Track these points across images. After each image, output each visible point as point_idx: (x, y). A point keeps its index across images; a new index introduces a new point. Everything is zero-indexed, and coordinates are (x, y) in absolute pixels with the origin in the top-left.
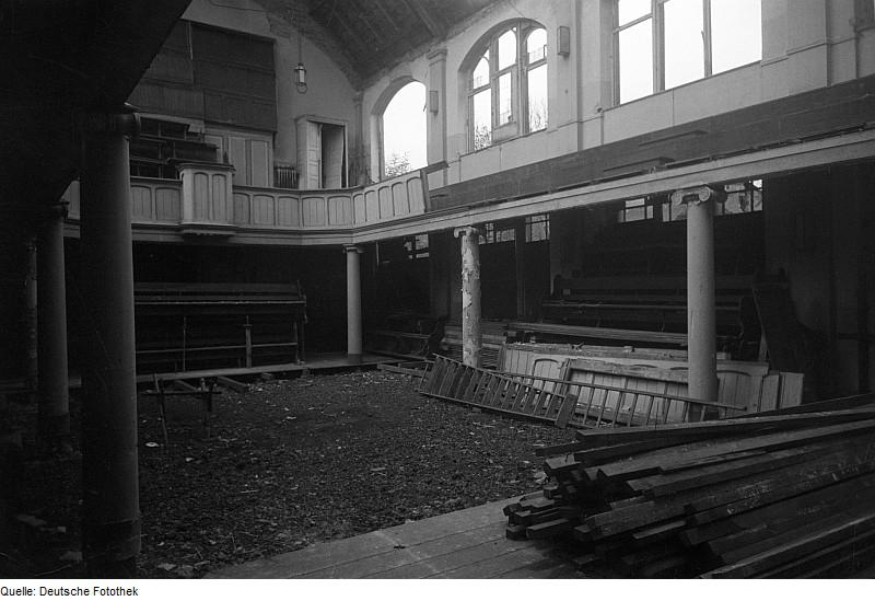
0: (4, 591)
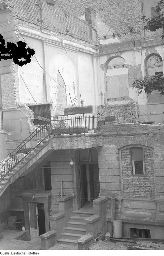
0: (1, 253)
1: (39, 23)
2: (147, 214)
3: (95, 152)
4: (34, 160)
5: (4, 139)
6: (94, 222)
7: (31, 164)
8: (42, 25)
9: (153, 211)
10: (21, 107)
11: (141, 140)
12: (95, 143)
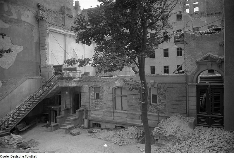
1: (63, 26)
2: (100, 117)
3: (79, 88)
4: (51, 91)
5: (41, 81)
6: (74, 120)
7: (49, 93)
8: (65, 27)
9: (103, 116)
10: (49, 66)
11: (98, 84)
12: (78, 84)
